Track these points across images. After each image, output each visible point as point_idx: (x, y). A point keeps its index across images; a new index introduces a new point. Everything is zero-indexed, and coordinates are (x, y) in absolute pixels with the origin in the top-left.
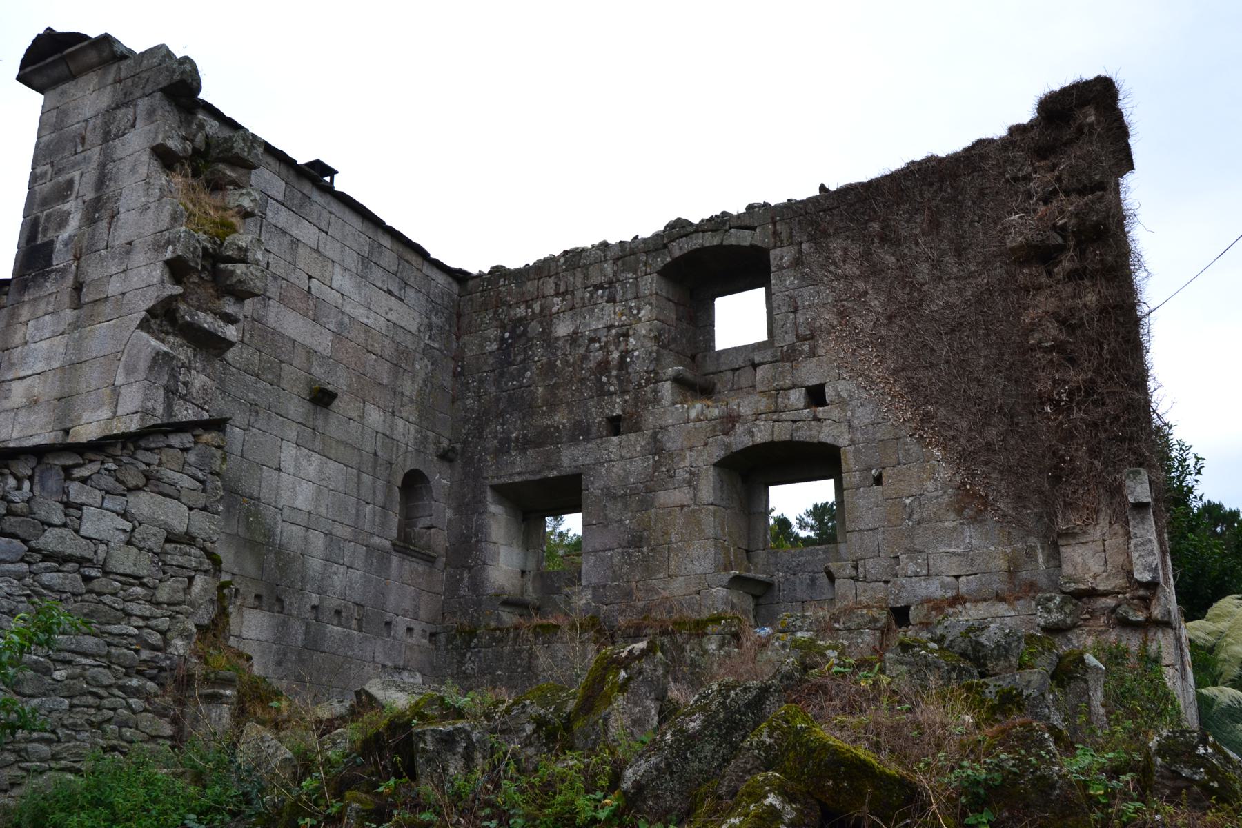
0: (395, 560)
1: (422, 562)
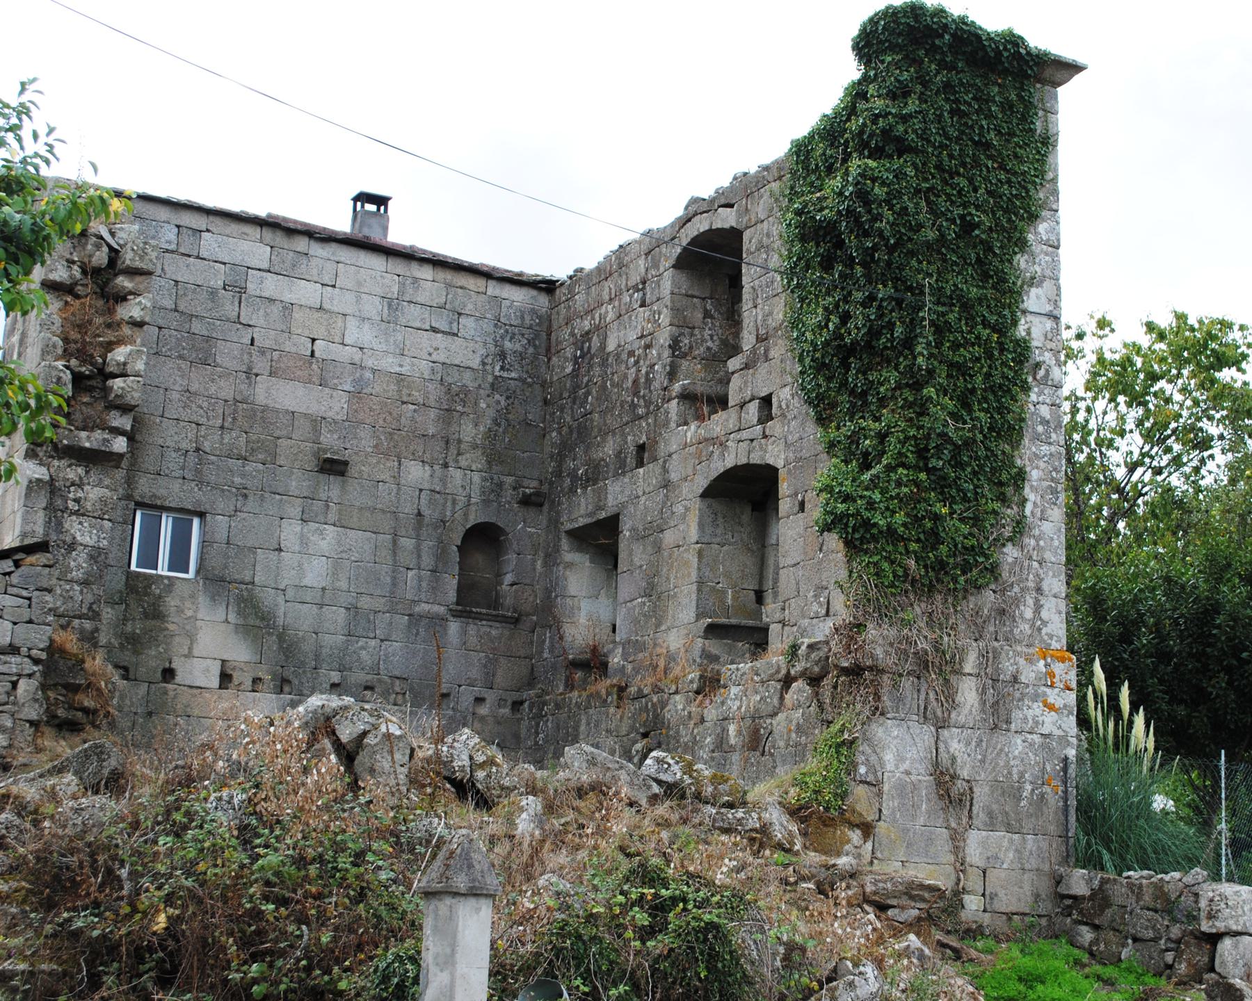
0: (454, 627)
1: (498, 625)
